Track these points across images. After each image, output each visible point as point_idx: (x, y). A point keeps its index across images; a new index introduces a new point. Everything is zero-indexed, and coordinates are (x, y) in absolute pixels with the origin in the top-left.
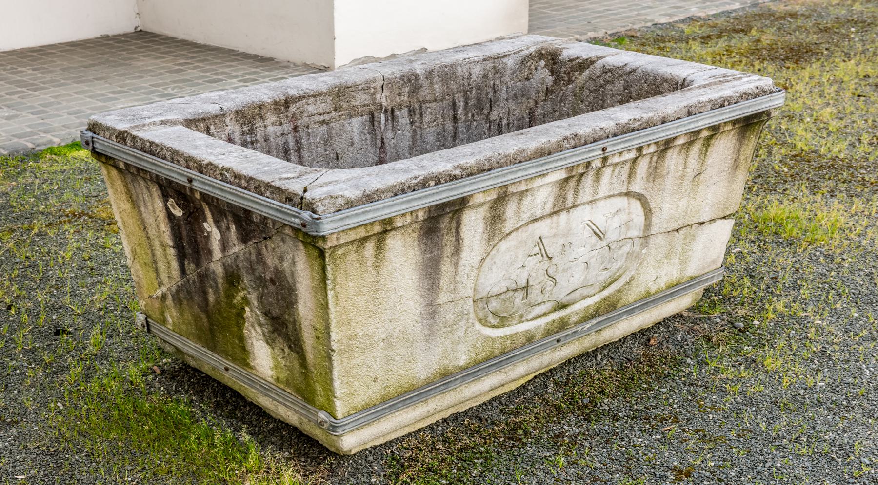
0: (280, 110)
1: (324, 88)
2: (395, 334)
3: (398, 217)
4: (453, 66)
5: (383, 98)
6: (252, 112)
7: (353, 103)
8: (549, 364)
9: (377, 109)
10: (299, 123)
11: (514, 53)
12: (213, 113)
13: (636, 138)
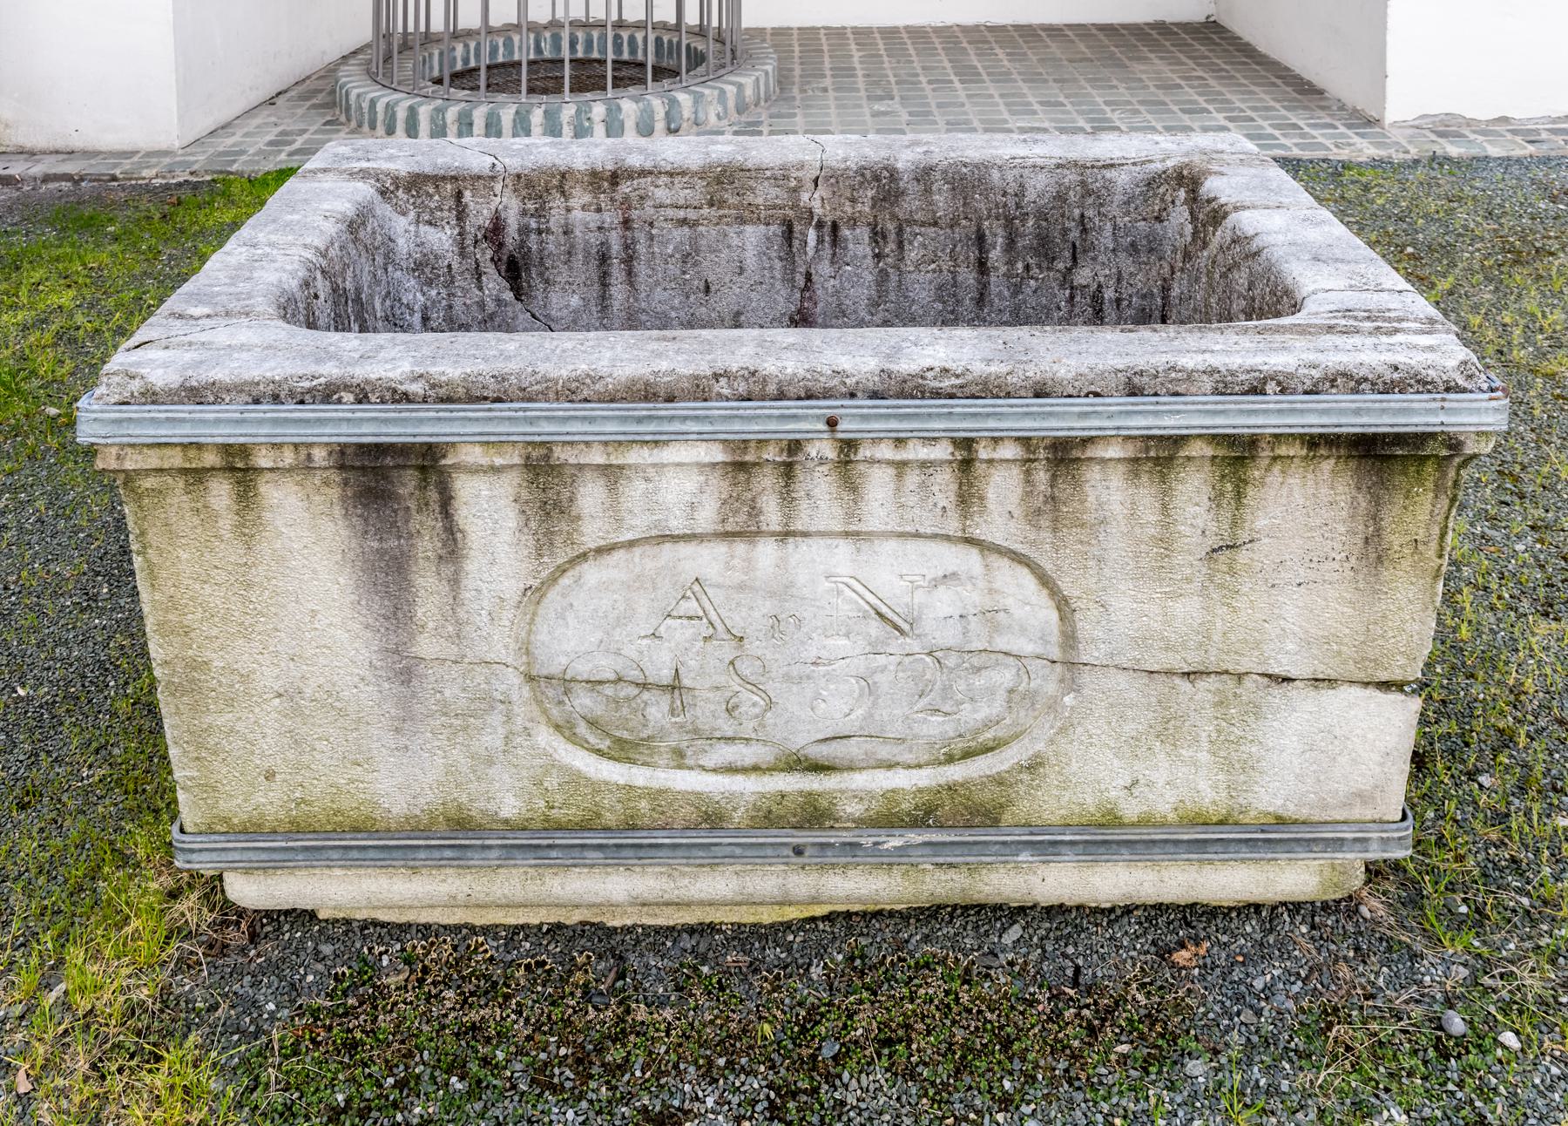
0: (599, 188)
1: (695, 161)
2: (308, 692)
3: (263, 447)
4: (983, 167)
5: (815, 200)
6: (547, 182)
7: (750, 198)
8: (848, 899)
9: (802, 218)
10: (635, 214)
11: (1134, 164)
12: (476, 171)
13: (939, 415)
